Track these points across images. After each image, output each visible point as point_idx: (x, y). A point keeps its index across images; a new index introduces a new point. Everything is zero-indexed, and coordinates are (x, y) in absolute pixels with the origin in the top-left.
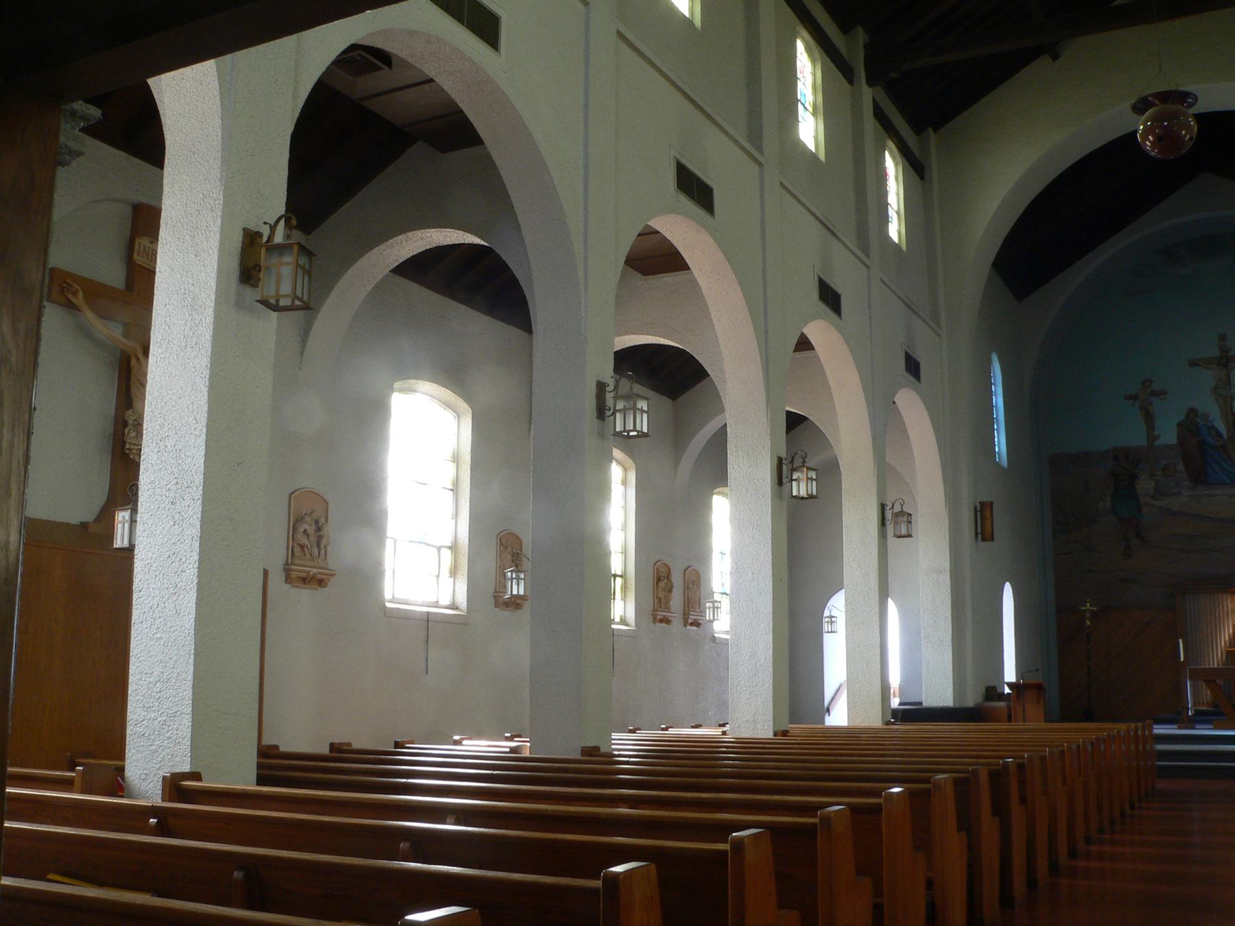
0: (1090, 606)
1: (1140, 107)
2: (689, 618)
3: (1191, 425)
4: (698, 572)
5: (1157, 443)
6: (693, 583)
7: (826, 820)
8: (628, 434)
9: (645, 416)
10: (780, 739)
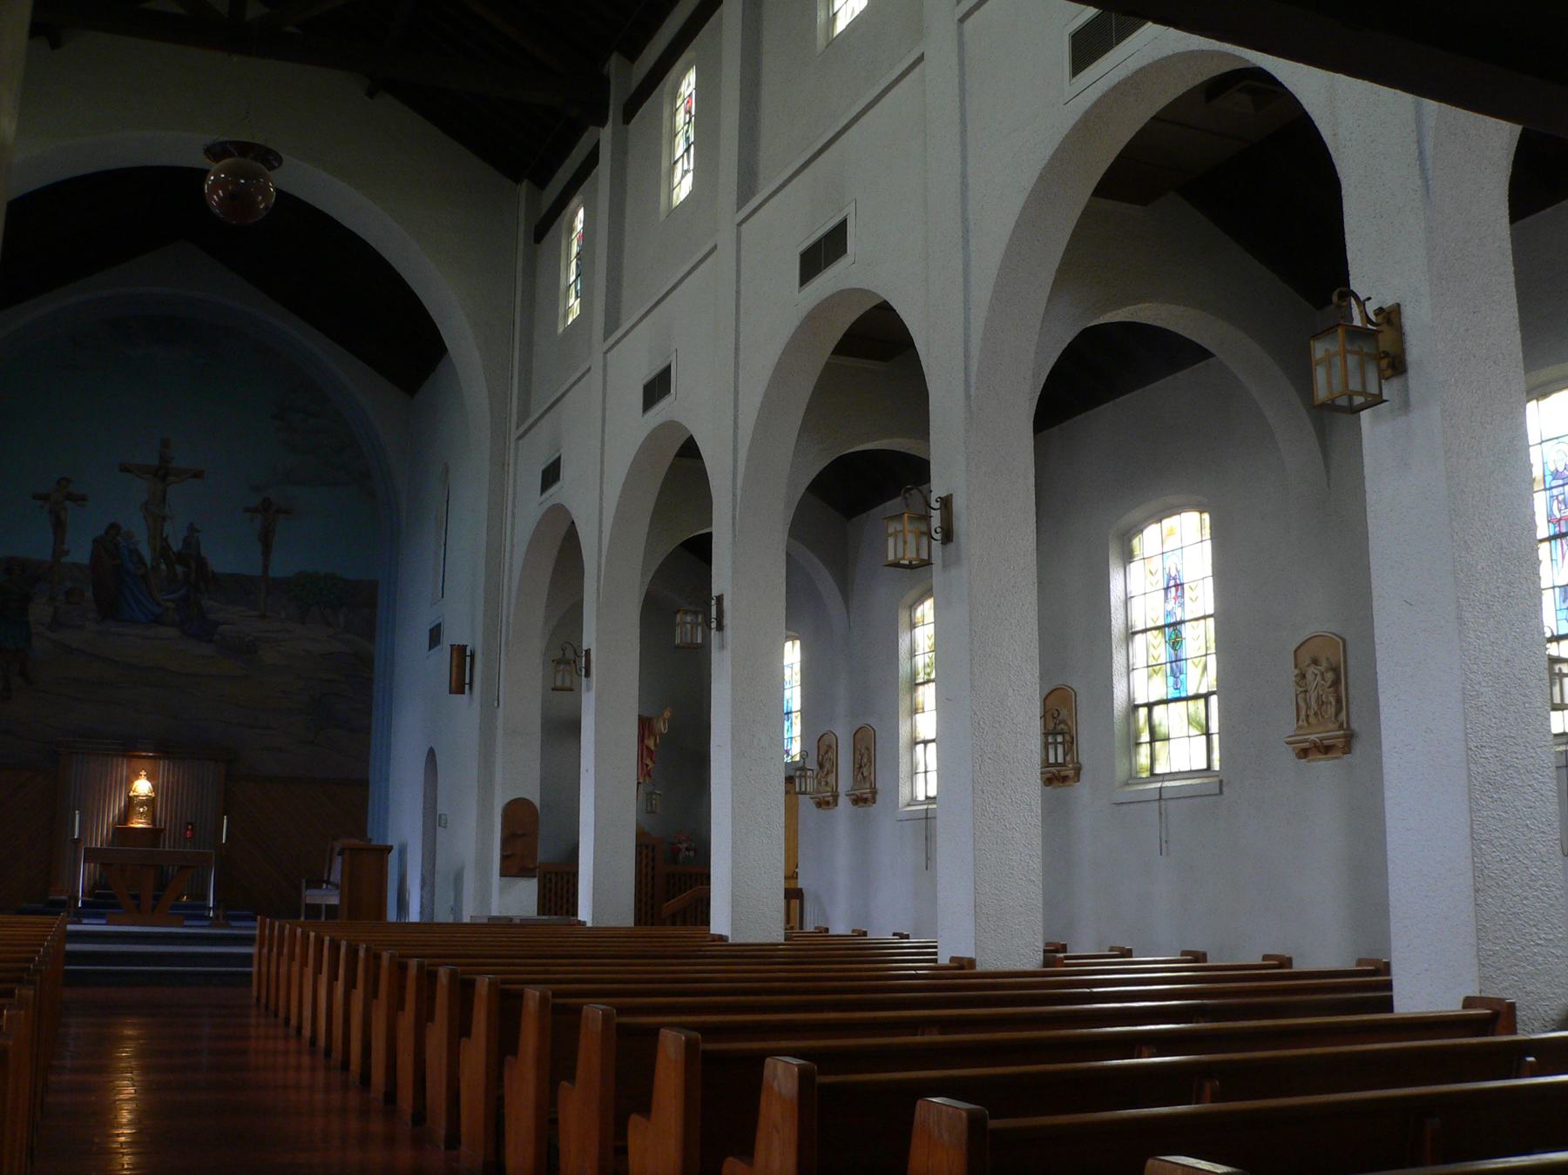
1: (216, 152)
3: (110, 544)
5: (62, 560)
10: (896, 939)
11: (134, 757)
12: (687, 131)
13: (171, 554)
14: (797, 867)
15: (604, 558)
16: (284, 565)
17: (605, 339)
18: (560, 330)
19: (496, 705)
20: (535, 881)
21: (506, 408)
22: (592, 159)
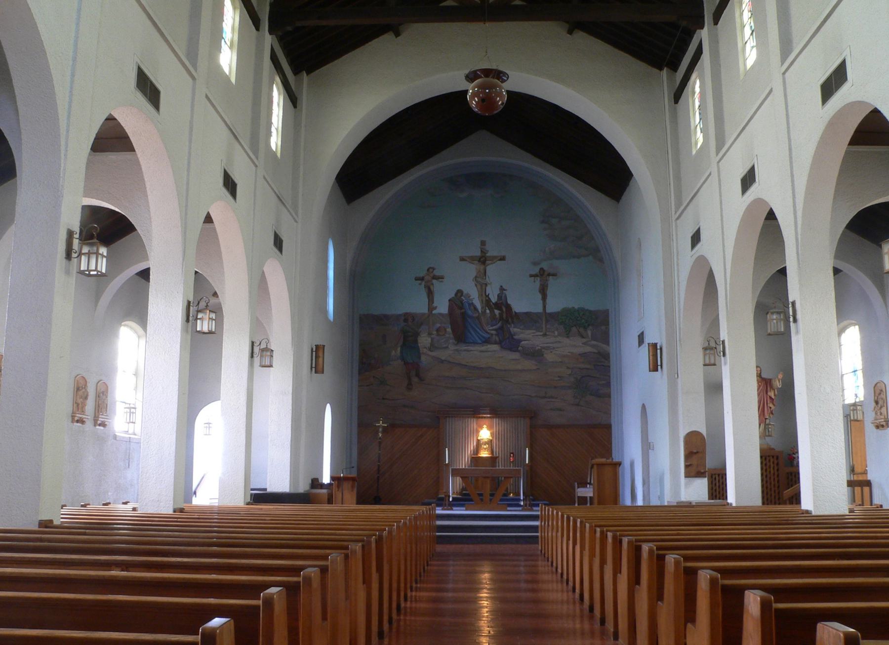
0: (382, 423)
1: (471, 77)
2: (98, 420)
3: (458, 302)
4: (106, 385)
5: (434, 312)
6: (103, 393)
8: (89, 273)
9: (105, 260)
10: (178, 515)
11: (480, 417)
12: (750, 23)
13: (492, 303)
14: (867, 467)
15: (728, 285)
16: (555, 305)
18: (694, 152)
19: (676, 376)
20: (706, 480)
21: (668, 202)
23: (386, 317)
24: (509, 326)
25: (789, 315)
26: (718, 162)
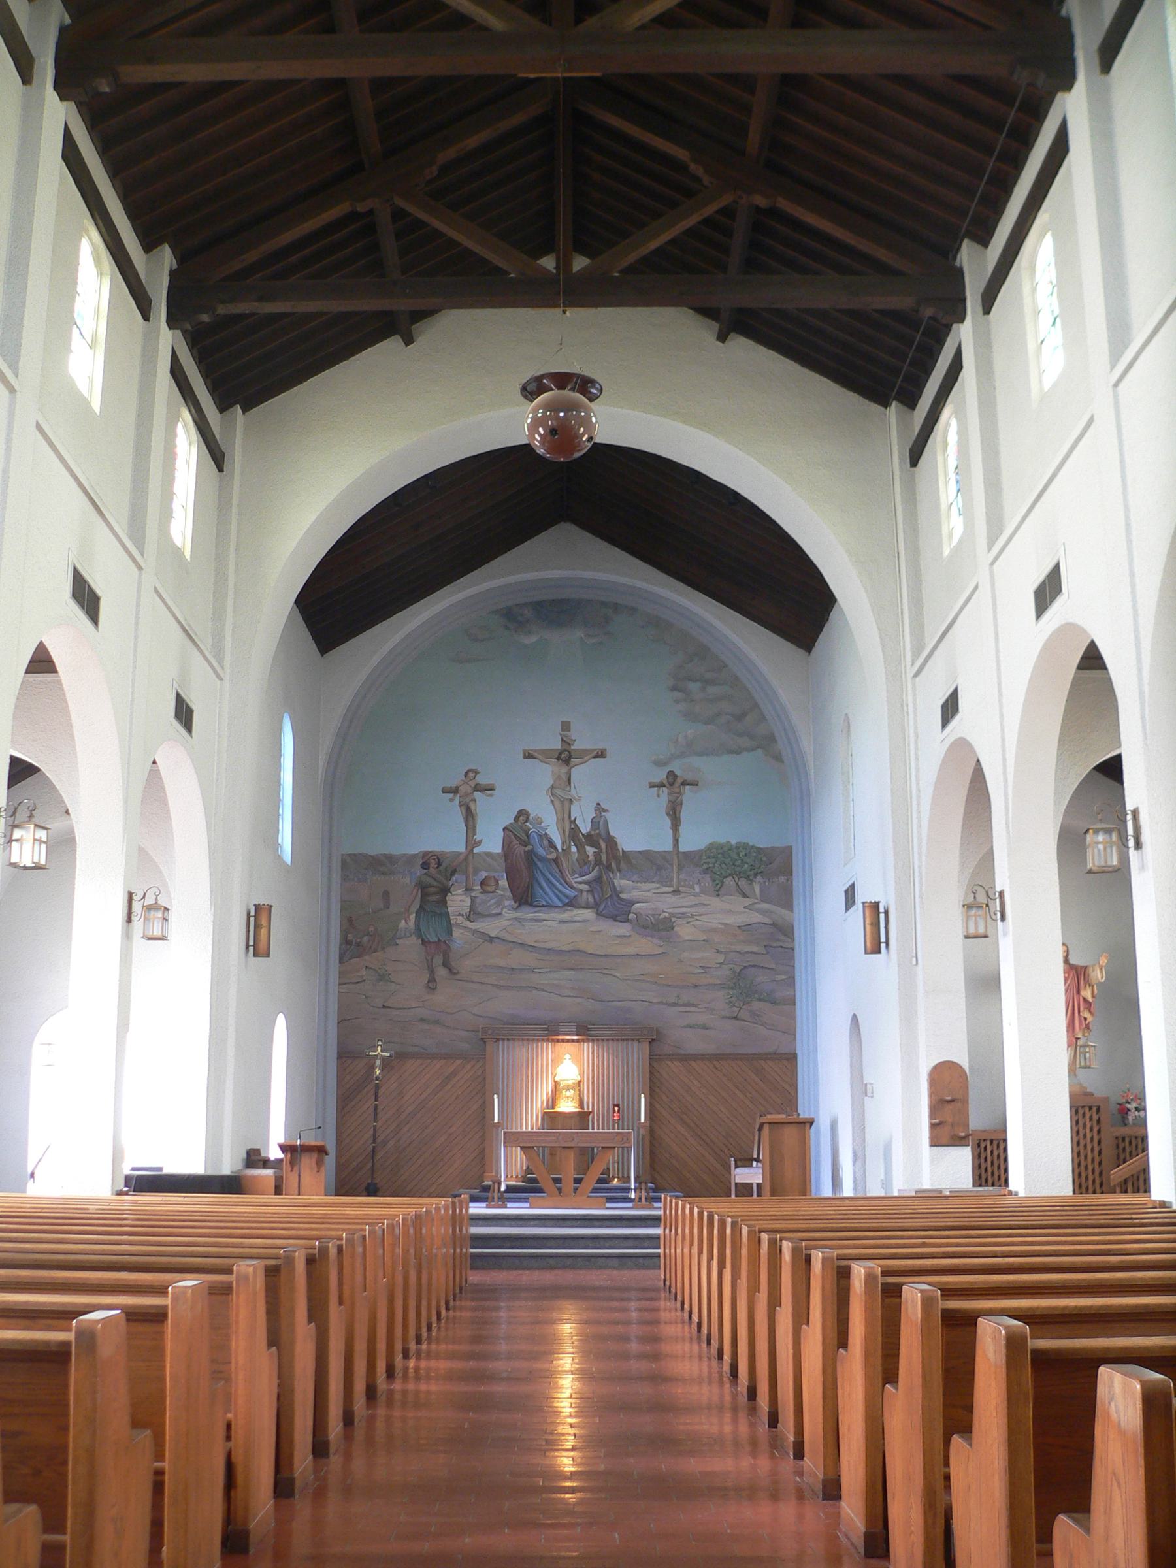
5: (476, 850)
7: (88, 1337)
11: (558, 1041)
16: (694, 839)
17: (989, 550)
18: (946, 552)
19: (914, 963)
22: (956, 366)
23: (390, 858)
24: (611, 875)
25: (1127, 836)
26: (992, 564)
